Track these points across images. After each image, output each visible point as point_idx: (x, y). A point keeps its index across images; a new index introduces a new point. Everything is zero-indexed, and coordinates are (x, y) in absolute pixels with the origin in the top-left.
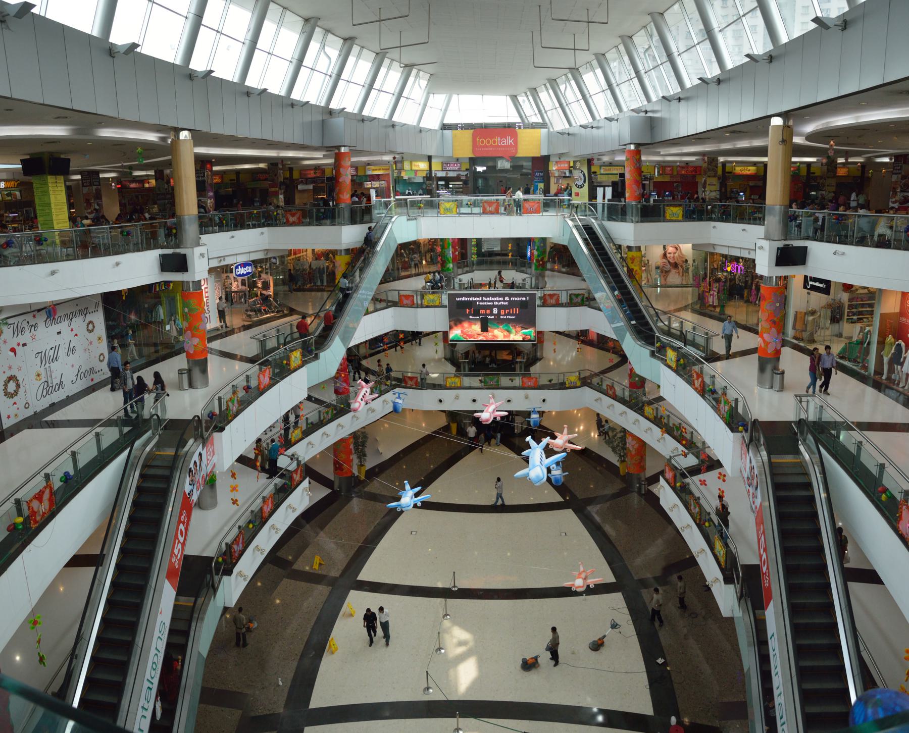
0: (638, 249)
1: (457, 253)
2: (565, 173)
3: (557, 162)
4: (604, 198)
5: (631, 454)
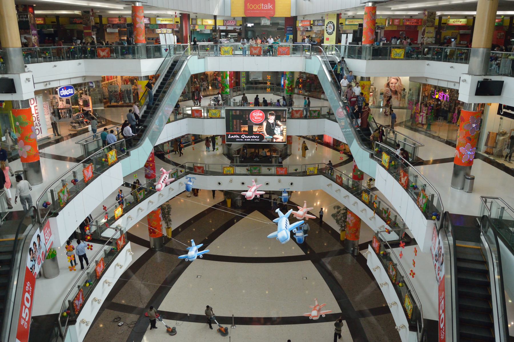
0: (369, 79)
1: (233, 82)
2: (307, 28)
3: (302, 21)
4: (347, 41)
5: (349, 226)
